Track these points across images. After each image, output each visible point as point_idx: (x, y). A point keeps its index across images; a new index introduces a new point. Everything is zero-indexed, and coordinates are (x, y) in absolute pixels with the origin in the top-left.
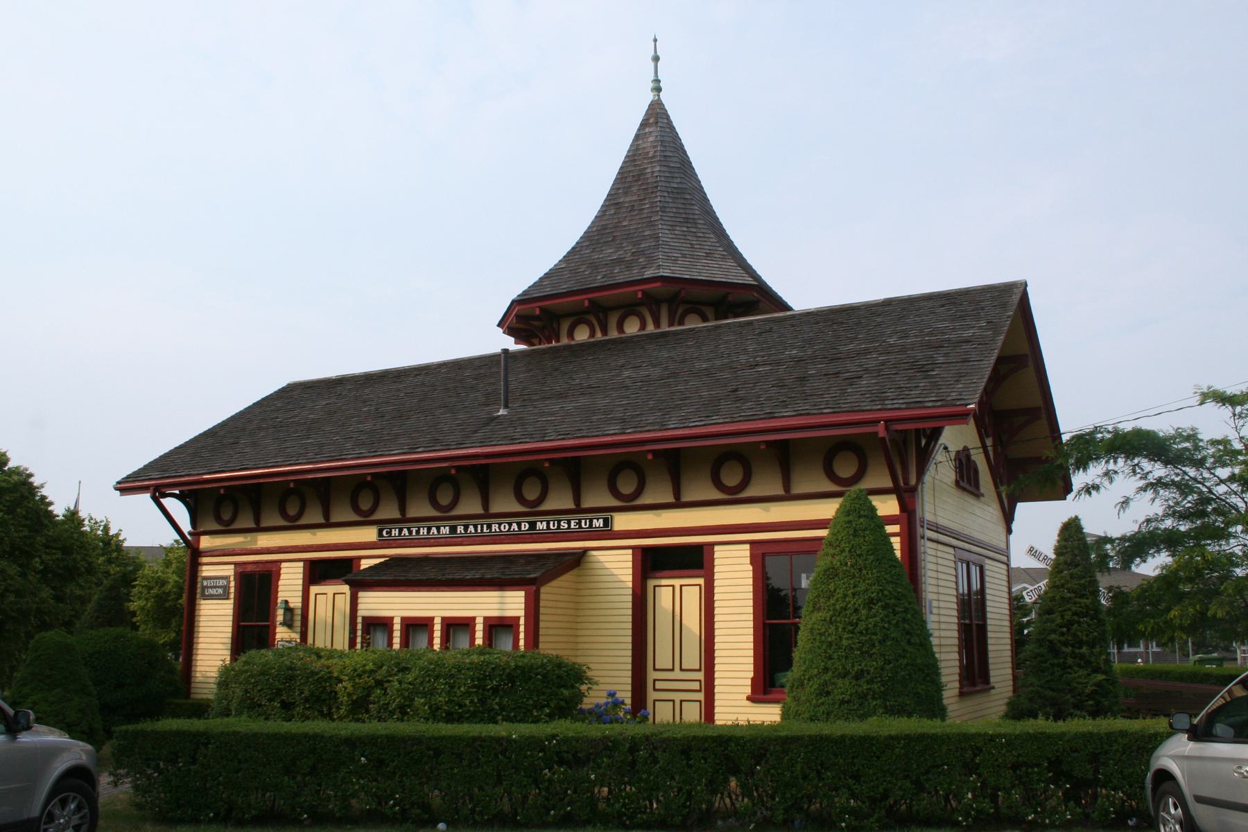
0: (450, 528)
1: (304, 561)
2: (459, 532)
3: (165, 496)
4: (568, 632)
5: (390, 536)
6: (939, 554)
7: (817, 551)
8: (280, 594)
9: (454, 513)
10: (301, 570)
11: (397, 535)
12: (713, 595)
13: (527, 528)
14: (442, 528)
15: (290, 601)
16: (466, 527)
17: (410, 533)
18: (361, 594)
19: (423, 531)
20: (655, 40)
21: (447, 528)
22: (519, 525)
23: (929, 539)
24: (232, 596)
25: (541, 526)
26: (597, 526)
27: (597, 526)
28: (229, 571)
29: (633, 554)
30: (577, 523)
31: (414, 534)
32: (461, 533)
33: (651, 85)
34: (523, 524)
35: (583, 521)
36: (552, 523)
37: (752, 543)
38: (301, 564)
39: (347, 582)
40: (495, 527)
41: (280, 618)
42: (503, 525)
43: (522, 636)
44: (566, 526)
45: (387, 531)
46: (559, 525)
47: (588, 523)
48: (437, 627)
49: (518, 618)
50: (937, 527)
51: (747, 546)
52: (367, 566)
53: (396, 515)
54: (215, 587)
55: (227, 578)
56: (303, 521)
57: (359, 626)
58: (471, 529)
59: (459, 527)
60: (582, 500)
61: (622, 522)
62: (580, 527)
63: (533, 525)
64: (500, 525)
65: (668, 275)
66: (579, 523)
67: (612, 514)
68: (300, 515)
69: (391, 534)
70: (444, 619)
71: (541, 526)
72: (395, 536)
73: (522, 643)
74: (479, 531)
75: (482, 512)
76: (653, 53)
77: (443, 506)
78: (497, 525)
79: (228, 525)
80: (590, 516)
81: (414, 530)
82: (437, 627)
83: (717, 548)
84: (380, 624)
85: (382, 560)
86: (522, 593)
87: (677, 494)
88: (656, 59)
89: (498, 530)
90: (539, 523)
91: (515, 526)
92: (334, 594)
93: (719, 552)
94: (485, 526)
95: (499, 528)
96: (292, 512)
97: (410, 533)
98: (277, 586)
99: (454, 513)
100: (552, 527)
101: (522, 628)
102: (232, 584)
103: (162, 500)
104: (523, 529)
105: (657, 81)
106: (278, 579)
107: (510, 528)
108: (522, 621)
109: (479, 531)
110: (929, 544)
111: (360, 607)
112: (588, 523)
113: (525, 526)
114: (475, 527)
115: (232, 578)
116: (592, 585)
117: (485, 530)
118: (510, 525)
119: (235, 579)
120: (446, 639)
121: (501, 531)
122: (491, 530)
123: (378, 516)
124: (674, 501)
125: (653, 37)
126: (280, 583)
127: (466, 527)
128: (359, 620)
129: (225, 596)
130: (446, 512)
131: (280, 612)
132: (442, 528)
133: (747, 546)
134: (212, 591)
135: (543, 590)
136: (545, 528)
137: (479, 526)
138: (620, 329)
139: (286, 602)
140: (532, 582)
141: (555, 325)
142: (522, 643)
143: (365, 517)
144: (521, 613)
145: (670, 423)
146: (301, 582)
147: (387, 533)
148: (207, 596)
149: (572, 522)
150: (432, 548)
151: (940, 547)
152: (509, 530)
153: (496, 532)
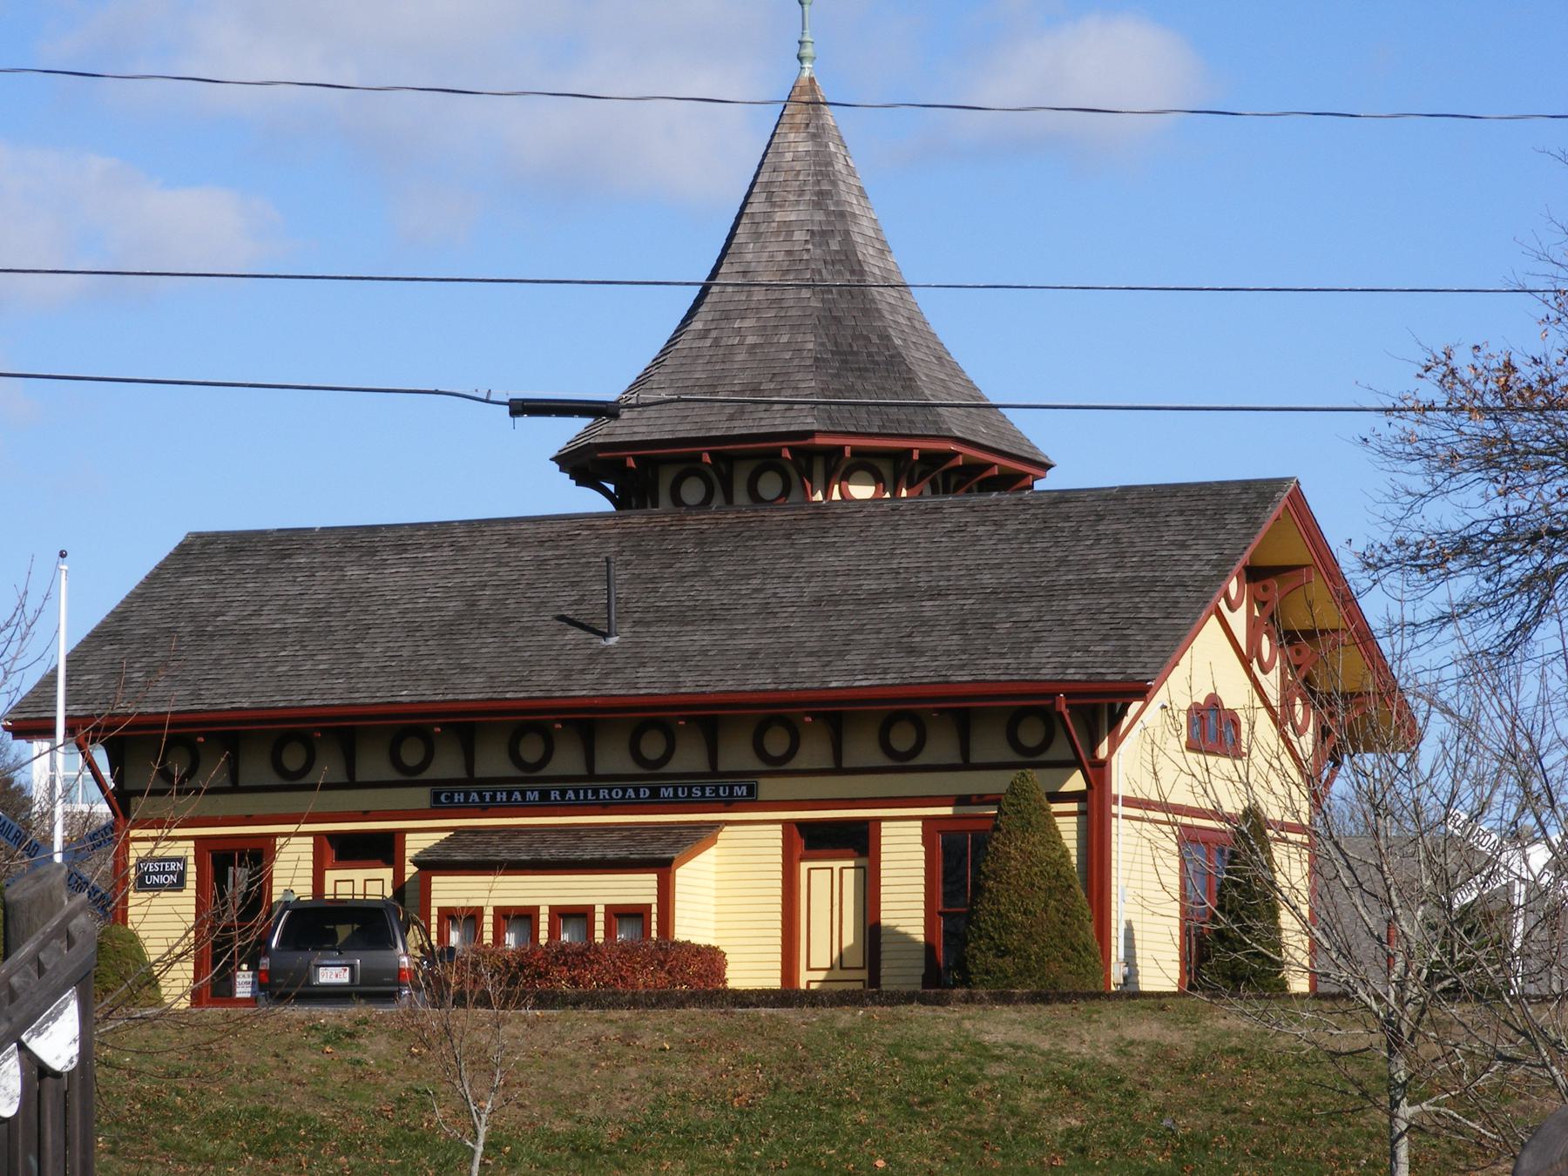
0: (540, 794)
2: (553, 798)
5: (598, 798)
7: (68, 931)
9: (544, 772)
13: (647, 795)
14: (529, 793)
17: (482, 797)
21: (536, 793)
22: (637, 791)
23: (1124, 817)
26: (740, 794)
27: (740, 794)
28: (187, 850)
30: (714, 791)
31: (488, 800)
34: (642, 790)
35: (721, 788)
36: (680, 789)
37: (924, 819)
44: (699, 794)
45: (446, 796)
46: (690, 792)
49: (650, 906)
53: (578, 768)
54: (164, 873)
56: (921, 760)
62: (718, 795)
63: (655, 792)
64: (610, 790)
66: (716, 791)
74: (582, 798)
75: (346, 780)
83: (883, 824)
85: (447, 834)
86: (654, 876)
87: (965, 751)
89: (607, 797)
90: (663, 790)
92: (353, 881)
93: (886, 827)
94: (590, 791)
95: (610, 794)
99: (544, 772)
100: (680, 795)
102: (192, 869)
104: (642, 796)
108: (654, 909)
109: (582, 798)
114: (577, 793)
115: (191, 860)
117: (590, 797)
118: (625, 791)
121: (611, 798)
122: (598, 796)
123: (432, 773)
129: (179, 885)
132: (736, 788)
133: (919, 823)
136: (671, 795)
137: (582, 792)
145: (831, 679)
147: (447, 798)
148: (151, 885)
149: (707, 789)
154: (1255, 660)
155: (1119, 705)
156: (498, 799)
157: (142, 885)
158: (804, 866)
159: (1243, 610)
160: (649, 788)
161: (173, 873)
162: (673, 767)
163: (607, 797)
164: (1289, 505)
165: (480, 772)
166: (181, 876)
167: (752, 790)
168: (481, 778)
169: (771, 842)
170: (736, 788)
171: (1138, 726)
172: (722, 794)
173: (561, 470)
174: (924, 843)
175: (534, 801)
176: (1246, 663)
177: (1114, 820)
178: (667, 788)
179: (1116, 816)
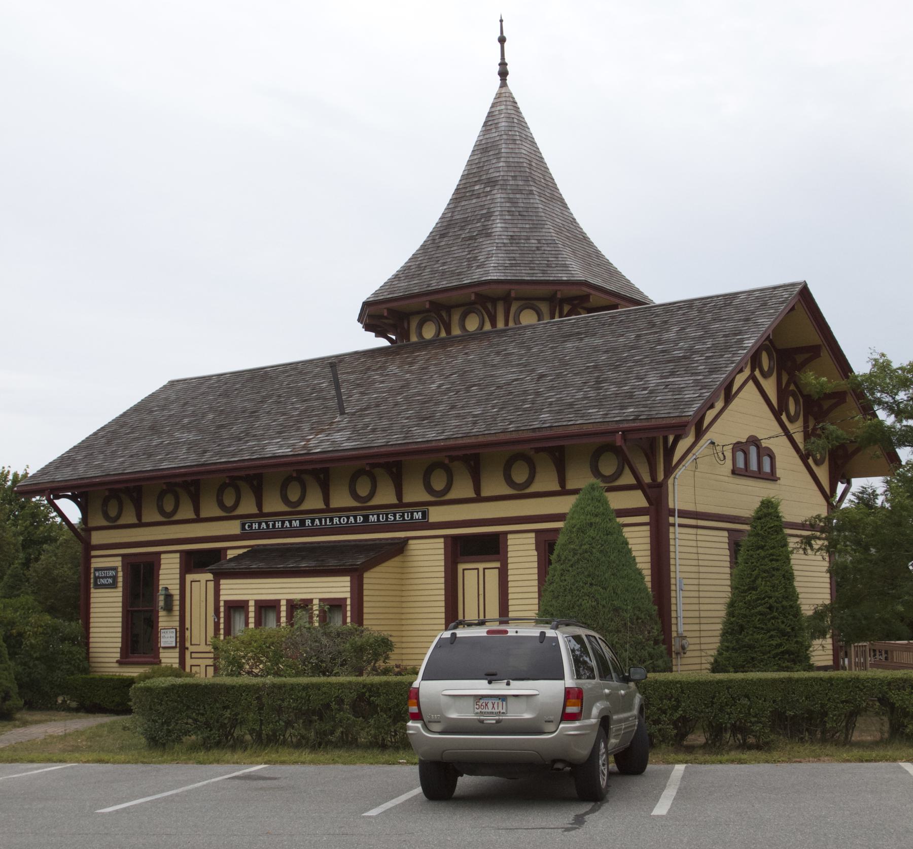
0: (422, 514)
1: (445, 537)
2: (307, 525)
3: (58, 497)
4: (395, 610)
5: (252, 529)
6: (699, 538)
8: (161, 582)
9: (372, 503)
10: (178, 560)
11: (280, 527)
12: (507, 576)
14: (293, 522)
15: (169, 588)
16: (313, 521)
17: (268, 526)
18: (222, 581)
19: (278, 525)
20: (501, 21)
21: (298, 521)
23: (680, 526)
24: (120, 584)
25: (373, 518)
26: (417, 518)
27: (417, 518)
28: (117, 562)
29: (445, 543)
31: (271, 527)
32: (309, 526)
33: (497, 68)
34: (358, 517)
35: (406, 514)
36: (381, 516)
37: (536, 531)
38: (178, 555)
39: (211, 571)
40: (336, 520)
41: (161, 604)
42: (342, 519)
43: (349, 614)
44: (393, 518)
45: (249, 525)
46: (387, 517)
47: (410, 516)
48: (252, 609)
49: (345, 599)
50: (697, 515)
51: (533, 535)
52: (232, 556)
53: (392, 499)
54: (106, 577)
55: (115, 569)
56: (533, 489)
57: (222, 609)
58: (317, 522)
59: (307, 521)
60: (331, 501)
61: (437, 514)
62: (404, 519)
63: (366, 518)
64: (340, 518)
65: (496, 278)
67: (429, 508)
68: (175, 511)
69: (252, 527)
70: (257, 602)
71: (373, 518)
72: (255, 529)
73: (349, 620)
74: (323, 524)
76: (499, 35)
77: (291, 502)
78: (338, 519)
79: (231, 512)
80: (411, 509)
81: (271, 524)
82: (252, 609)
83: (509, 536)
84: (238, 607)
85: (245, 550)
86: (348, 578)
87: (477, 489)
88: (502, 40)
89: (338, 523)
90: (371, 516)
91: (352, 519)
93: (512, 540)
94: (328, 519)
95: (340, 521)
96: (169, 508)
97: (268, 526)
98: (158, 575)
99: (372, 503)
100: (381, 520)
101: (349, 608)
102: (120, 574)
103: (56, 501)
104: (358, 521)
105: (503, 64)
106: (159, 569)
107: (348, 521)
108: (349, 602)
109: (323, 524)
110: (678, 529)
111: (222, 592)
112: (410, 516)
113: (360, 519)
115: (120, 569)
116: (413, 570)
118: (348, 518)
119: (123, 570)
120: (290, 616)
122: (333, 522)
123: (240, 511)
124: (560, 489)
125: (500, 19)
126: (161, 572)
127: (313, 521)
128: (222, 604)
129: (114, 585)
130: (440, 497)
131: (162, 598)
132: (415, 513)
133: (533, 535)
134: (103, 581)
135: (366, 575)
136: (376, 520)
137: (323, 520)
138: (463, 327)
139: (166, 589)
140: (356, 570)
141: (406, 325)
142: (349, 620)
143: (168, 518)
144: (348, 595)
146: (178, 571)
147: (249, 526)
148: (100, 585)
149: (397, 515)
150: (231, 546)
151: (700, 531)
152: (347, 523)
153: (337, 524)
154: (784, 414)
155: (671, 439)
156: (277, 527)
157: (97, 586)
158: (461, 567)
159: (800, 423)
160: (363, 516)
161: (110, 577)
162: (375, 501)
163: (338, 523)
164: (801, 300)
165: (407, 499)
166: (115, 578)
167: (425, 514)
168: (145, 523)
169: (116, 610)
170: (415, 513)
171: (690, 457)
172: (406, 518)
173: (376, 336)
174: (537, 549)
175: (374, 522)
176: (777, 415)
177: (671, 529)
178: (373, 515)
179: (674, 525)
